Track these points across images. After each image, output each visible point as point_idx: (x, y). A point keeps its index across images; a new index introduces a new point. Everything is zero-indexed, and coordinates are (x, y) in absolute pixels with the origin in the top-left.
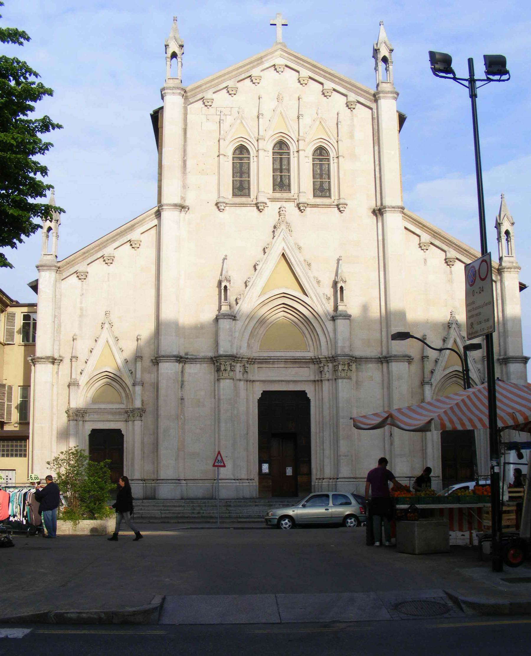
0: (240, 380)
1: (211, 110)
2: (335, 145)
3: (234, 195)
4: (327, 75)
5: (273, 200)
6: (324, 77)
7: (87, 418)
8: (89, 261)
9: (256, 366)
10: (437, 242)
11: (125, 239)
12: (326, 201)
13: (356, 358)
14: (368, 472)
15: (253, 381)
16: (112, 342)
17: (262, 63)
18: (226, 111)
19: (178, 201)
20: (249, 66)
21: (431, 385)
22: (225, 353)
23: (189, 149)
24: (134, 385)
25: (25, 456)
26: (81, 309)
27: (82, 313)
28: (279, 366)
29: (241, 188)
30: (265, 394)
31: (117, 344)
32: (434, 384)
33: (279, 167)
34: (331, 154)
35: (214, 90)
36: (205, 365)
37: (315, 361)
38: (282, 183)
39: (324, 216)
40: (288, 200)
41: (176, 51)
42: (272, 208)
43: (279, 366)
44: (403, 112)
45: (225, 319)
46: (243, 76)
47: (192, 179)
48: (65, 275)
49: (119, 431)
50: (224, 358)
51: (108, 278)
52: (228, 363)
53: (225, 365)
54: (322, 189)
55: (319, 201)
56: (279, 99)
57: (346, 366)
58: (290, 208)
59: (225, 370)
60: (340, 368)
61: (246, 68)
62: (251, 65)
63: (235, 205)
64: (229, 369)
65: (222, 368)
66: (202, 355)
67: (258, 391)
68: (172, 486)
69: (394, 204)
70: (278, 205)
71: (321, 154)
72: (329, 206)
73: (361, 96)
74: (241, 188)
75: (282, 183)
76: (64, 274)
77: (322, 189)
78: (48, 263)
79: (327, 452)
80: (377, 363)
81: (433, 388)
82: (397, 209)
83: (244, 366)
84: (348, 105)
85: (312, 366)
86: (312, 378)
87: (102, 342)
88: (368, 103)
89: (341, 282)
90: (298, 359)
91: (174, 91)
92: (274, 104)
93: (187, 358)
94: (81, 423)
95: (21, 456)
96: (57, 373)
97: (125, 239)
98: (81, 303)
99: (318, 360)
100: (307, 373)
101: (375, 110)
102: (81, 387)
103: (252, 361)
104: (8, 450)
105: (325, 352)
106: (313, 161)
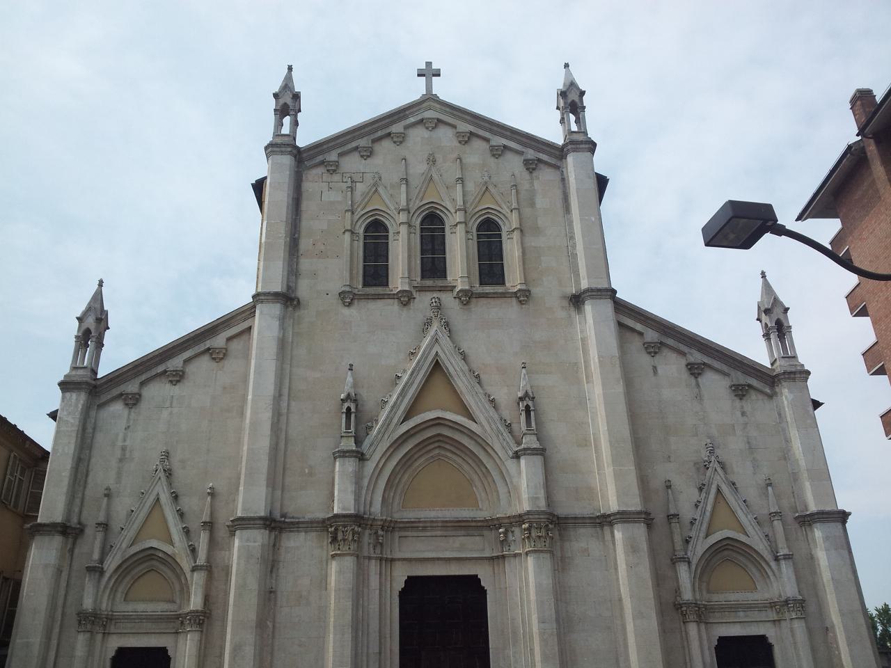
0: (370, 558)
3: (365, 284)
4: (495, 128)
5: (421, 289)
6: (491, 131)
8: (144, 377)
10: (481, 132)
11: (202, 347)
13: (558, 518)
15: (392, 560)
18: (356, 178)
20: (387, 121)
21: (689, 563)
22: (344, 512)
23: (305, 224)
24: (194, 569)
26: (124, 449)
27: (124, 455)
28: (434, 533)
29: (375, 271)
30: (411, 581)
32: (694, 562)
33: (430, 247)
34: (503, 228)
35: (339, 151)
36: (314, 534)
41: (288, 103)
43: (434, 533)
45: (346, 457)
48: (104, 398)
50: (343, 519)
51: (171, 403)
52: (349, 528)
54: (490, 266)
56: (432, 161)
57: (543, 530)
59: (344, 540)
61: (383, 122)
62: (391, 120)
64: (351, 538)
65: (340, 536)
66: (308, 517)
67: (400, 576)
73: (543, 152)
74: (375, 271)
76: (102, 397)
77: (490, 266)
80: (595, 527)
81: (694, 567)
82: (605, 293)
83: (376, 533)
84: (527, 163)
89: (527, 399)
90: (464, 521)
91: (283, 149)
93: (284, 522)
94: (99, 637)
96: (72, 551)
97: (202, 347)
98: (125, 440)
99: (496, 522)
102: (107, 575)
106: (478, 239)
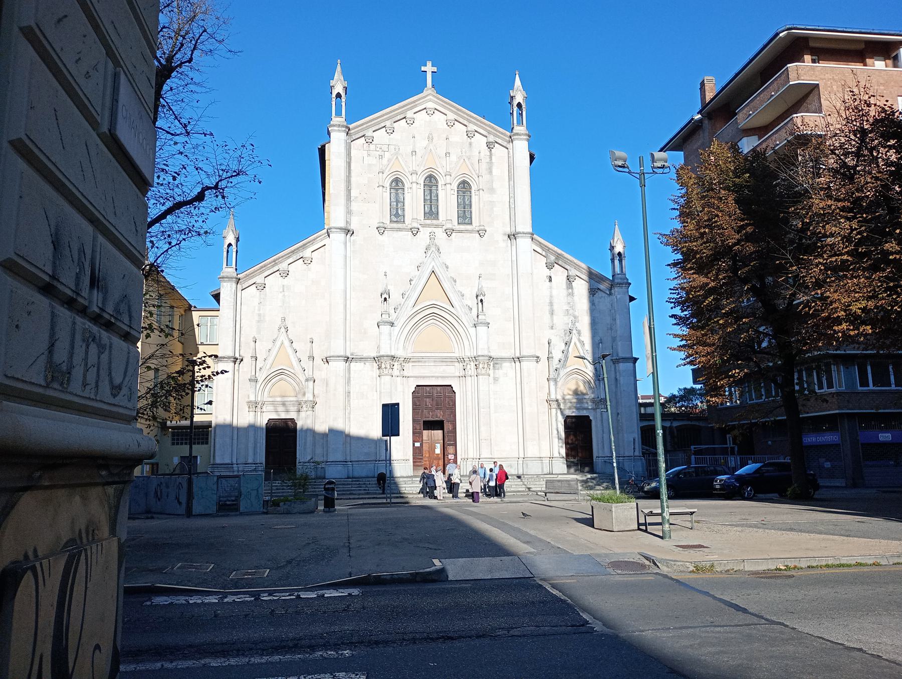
1: (372, 147)
2: (476, 179)
5: (424, 226)
7: (264, 409)
9: (411, 364)
12: (469, 227)
14: (339, 425)
16: (287, 343)
17: (416, 106)
19: (342, 224)
25: (207, 443)
26: (259, 315)
29: (397, 214)
31: (291, 346)
37: (461, 360)
38: (432, 213)
39: (466, 241)
40: (437, 226)
42: (424, 233)
44: (533, 152)
46: (399, 117)
47: (354, 206)
49: (588, 417)
53: (386, 363)
54: (465, 214)
55: (462, 227)
56: (430, 138)
58: (440, 233)
60: (481, 366)
63: (392, 229)
65: (383, 366)
68: (340, 468)
69: (525, 231)
70: (430, 230)
71: (464, 188)
72: (471, 232)
74: (397, 214)
75: (432, 213)
77: (465, 214)
78: (228, 275)
79: (470, 437)
85: (457, 364)
86: (457, 374)
87: (278, 343)
88: (505, 144)
92: (425, 143)
95: (203, 443)
100: (455, 369)
101: (511, 151)
103: (407, 360)
104: (178, 439)
105: (468, 354)
